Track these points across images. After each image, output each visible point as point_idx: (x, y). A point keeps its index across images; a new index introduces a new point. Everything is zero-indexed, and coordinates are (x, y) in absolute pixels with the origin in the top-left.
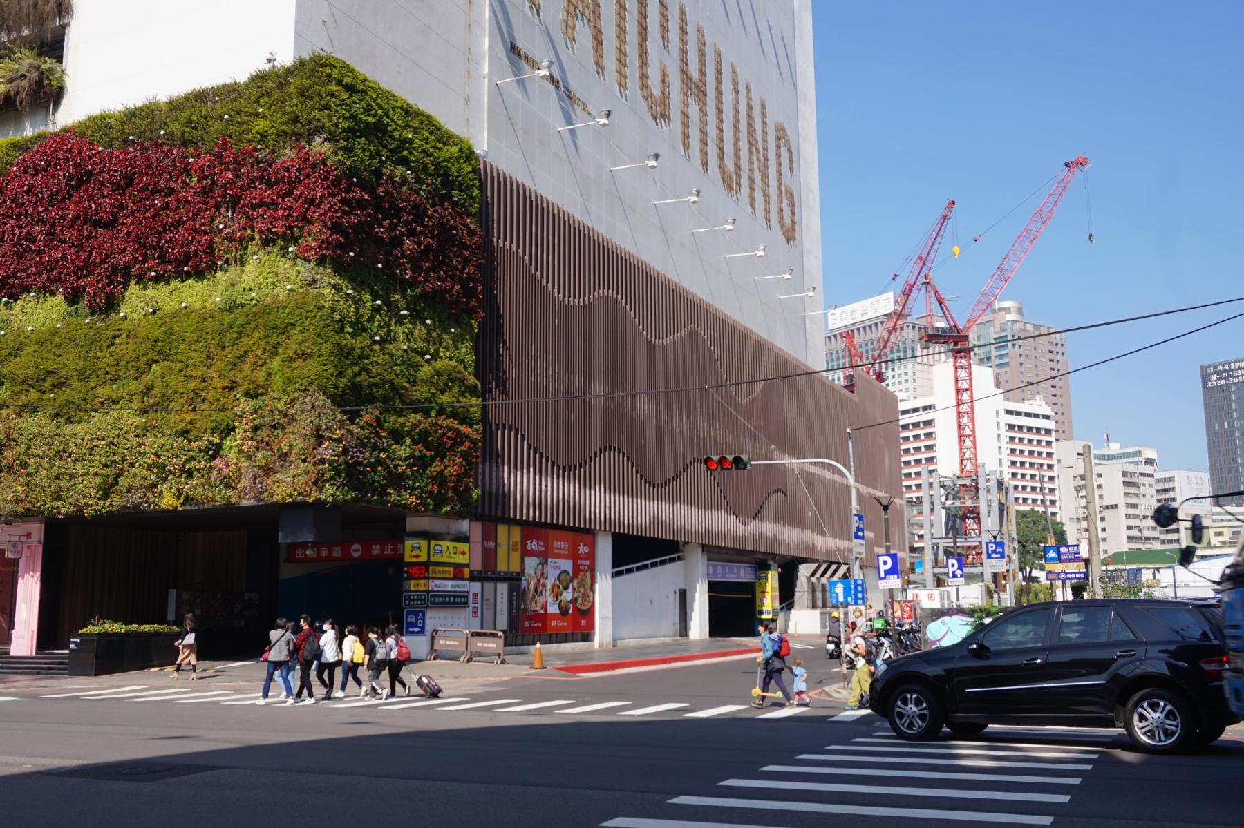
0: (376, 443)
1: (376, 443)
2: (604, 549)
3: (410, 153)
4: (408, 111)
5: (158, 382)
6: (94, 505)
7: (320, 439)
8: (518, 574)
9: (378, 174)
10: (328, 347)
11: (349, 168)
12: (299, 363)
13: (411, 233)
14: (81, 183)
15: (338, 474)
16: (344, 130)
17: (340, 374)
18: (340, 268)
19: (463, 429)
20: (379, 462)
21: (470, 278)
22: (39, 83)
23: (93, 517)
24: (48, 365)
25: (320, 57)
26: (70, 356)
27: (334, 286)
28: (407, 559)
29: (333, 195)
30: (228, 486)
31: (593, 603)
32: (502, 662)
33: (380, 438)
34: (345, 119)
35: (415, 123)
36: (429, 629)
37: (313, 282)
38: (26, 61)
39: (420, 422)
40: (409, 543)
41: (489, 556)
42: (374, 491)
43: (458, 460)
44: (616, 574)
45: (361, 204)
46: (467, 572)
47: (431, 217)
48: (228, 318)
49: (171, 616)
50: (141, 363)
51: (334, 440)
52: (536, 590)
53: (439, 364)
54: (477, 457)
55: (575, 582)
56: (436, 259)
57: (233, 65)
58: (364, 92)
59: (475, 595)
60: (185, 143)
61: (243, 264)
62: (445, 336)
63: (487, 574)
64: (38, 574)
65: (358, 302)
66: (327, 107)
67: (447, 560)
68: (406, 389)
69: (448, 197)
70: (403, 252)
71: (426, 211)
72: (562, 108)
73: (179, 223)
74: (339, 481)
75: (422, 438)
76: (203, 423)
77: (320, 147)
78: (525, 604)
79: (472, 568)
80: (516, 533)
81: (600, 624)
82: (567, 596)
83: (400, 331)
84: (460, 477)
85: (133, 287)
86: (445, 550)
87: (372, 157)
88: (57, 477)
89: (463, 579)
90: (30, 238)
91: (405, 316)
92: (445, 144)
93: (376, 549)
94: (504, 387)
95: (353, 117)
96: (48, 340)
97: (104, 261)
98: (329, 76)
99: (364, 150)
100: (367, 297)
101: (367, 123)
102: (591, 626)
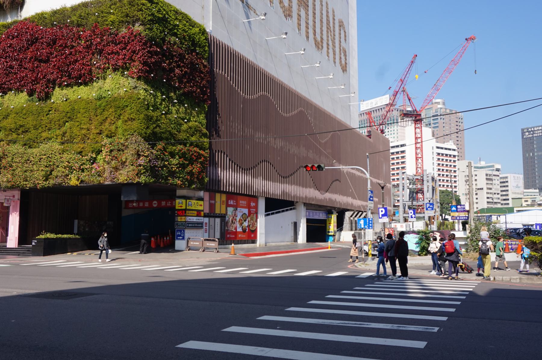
0: (163, 158)
1: (163, 158)
2: (262, 204)
3: (178, 31)
4: (177, 12)
5: (68, 131)
6: (42, 184)
7: (139, 156)
8: (225, 214)
9: (163, 40)
10: (142, 116)
11: (151, 37)
12: (130, 123)
13: (178, 66)
15: (147, 171)
16: (149, 20)
17: (148, 128)
19: (201, 152)
20: (165, 166)
21: (204, 86)
24: (21, 123)
27: (145, 89)
28: (177, 208)
29: (144, 49)
30: (99, 176)
31: (257, 227)
32: (218, 252)
33: (165, 155)
34: (149, 15)
35: (180, 17)
36: (186, 237)
39: (182, 149)
41: (212, 207)
42: (163, 178)
43: (199, 165)
45: (156, 53)
46: (202, 213)
47: (187, 59)
48: (99, 103)
49: (76, 231)
50: (61, 122)
51: (145, 156)
52: (232, 222)
53: (190, 124)
54: (207, 164)
56: (189, 77)
59: (206, 223)
60: (79, 26)
62: (193, 112)
63: (211, 215)
64: (18, 213)
65: (155, 96)
66: (141, 10)
68: (176, 135)
69: (195, 50)
70: (175, 75)
71: (185, 56)
73: (76, 61)
74: (147, 174)
75: (183, 156)
77: (138, 28)
80: (224, 197)
82: (246, 224)
83: (174, 109)
85: (57, 89)
86: (193, 204)
87: (161, 33)
88: (25, 171)
89: (201, 216)
90: (11, 67)
91: (176, 103)
92: (193, 27)
94: (219, 134)
95: (153, 14)
96: (20, 112)
97: (44, 78)
99: (157, 29)
102: (256, 237)
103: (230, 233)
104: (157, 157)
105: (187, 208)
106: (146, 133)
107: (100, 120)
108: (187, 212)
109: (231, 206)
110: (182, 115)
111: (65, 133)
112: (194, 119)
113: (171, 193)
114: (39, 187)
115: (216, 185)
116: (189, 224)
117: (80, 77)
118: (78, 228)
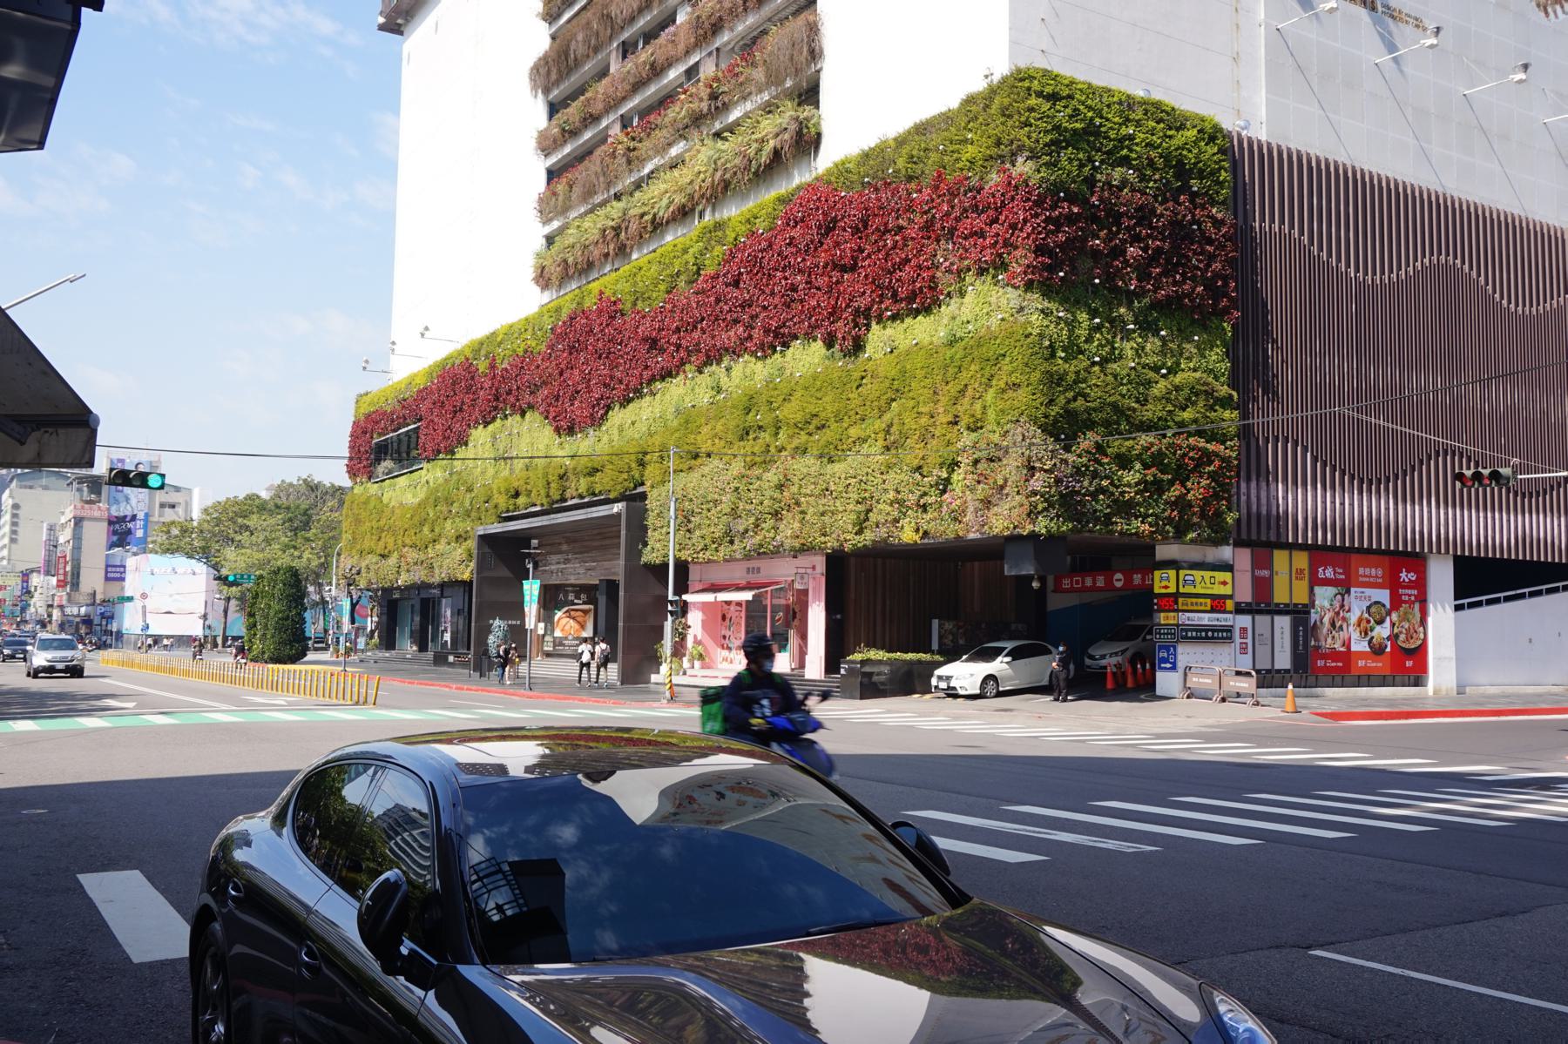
0: (1096, 470)
1: (1096, 470)
2: (1441, 576)
3: (1131, 150)
4: (1129, 103)
5: (896, 421)
6: (853, 541)
7: (1032, 469)
8: (1305, 606)
9: (1090, 182)
10: (1037, 375)
11: (1054, 184)
12: (1010, 394)
13: (1136, 239)
14: (829, 230)
15: (1051, 505)
16: (1046, 145)
17: (1051, 402)
18: (1048, 291)
19: (1211, 447)
20: (1103, 490)
21: (1216, 275)
22: (799, 134)
24: (812, 409)
25: (1019, 71)
26: (827, 399)
27: (1042, 311)
28: (1157, 590)
29: (1036, 216)
30: (955, 519)
31: (1425, 641)
32: (1257, 704)
33: (1102, 465)
34: (1046, 132)
35: (1138, 114)
36: (1181, 665)
37: (1021, 309)
38: (788, 114)
39: (1152, 444)
40: (1157, 574)
41: (1263, 587)
42: (1097, 521)
43: (1204, 482)
44: (1458, 608)
45: (1071, 219)
46: (1230, 604)
47: (1162, 215)
48: (949, 353)
49: (935, 646)
50: (882, 402)
52: (1333, 624)
53: (1178, 379)
54: (1230, 478)
55: (1394, 616)
56: (1168, 261)
57: (944, 97)
58: (1070, 97)
59: (1244, 630)
60: (910, 178)
61: (962, 294)
62: (1187, 346)
63: (1261, 604)
64: (823, 604)
65: (1072, 324)
66: (1027, 124)
68: (1134, 410)
69: (1186, 188)
70: (1126, 262)
71: (1153, 211)
72: (1380, 34)
73: (907, 261)
74: (1053, 512)
75: (1157, 460)
77: (1023, 167)
79: (1238, 599)
80: (1302, 560)
81: (1436, 667)
82: (1383, 632)
83: (1128, 348)
84: (1206, 502)
85: (874, 326)
86: (1199, 579)
87: (1081, 166)
88: (823, 514)
89: (1225, 612)
90: (794, 288)
91: (1134, 331)
92: (1178, 129)
93: (1100, 582)
94: (1275, 393)
95: (1057, 128)
96: (814, 385)
97: (848, 306)
98: (1029, 89)
99: (1070, 160)
100: (1083, 316)
101: (1075, 130)
102: (1422, 667)
103: (1325, 657)
104: (1078, 469)
105: (1182, 590)
106: (1046, 417)
107: (954, 392)
108: (1181, 600)
109: (1327, 582)
110: (1152, 359)
111: (890, 425)
113: (1141, 555)
114: (848, 547)
115: (1269, 528)
117: (911, 298)
118: (941, 637)
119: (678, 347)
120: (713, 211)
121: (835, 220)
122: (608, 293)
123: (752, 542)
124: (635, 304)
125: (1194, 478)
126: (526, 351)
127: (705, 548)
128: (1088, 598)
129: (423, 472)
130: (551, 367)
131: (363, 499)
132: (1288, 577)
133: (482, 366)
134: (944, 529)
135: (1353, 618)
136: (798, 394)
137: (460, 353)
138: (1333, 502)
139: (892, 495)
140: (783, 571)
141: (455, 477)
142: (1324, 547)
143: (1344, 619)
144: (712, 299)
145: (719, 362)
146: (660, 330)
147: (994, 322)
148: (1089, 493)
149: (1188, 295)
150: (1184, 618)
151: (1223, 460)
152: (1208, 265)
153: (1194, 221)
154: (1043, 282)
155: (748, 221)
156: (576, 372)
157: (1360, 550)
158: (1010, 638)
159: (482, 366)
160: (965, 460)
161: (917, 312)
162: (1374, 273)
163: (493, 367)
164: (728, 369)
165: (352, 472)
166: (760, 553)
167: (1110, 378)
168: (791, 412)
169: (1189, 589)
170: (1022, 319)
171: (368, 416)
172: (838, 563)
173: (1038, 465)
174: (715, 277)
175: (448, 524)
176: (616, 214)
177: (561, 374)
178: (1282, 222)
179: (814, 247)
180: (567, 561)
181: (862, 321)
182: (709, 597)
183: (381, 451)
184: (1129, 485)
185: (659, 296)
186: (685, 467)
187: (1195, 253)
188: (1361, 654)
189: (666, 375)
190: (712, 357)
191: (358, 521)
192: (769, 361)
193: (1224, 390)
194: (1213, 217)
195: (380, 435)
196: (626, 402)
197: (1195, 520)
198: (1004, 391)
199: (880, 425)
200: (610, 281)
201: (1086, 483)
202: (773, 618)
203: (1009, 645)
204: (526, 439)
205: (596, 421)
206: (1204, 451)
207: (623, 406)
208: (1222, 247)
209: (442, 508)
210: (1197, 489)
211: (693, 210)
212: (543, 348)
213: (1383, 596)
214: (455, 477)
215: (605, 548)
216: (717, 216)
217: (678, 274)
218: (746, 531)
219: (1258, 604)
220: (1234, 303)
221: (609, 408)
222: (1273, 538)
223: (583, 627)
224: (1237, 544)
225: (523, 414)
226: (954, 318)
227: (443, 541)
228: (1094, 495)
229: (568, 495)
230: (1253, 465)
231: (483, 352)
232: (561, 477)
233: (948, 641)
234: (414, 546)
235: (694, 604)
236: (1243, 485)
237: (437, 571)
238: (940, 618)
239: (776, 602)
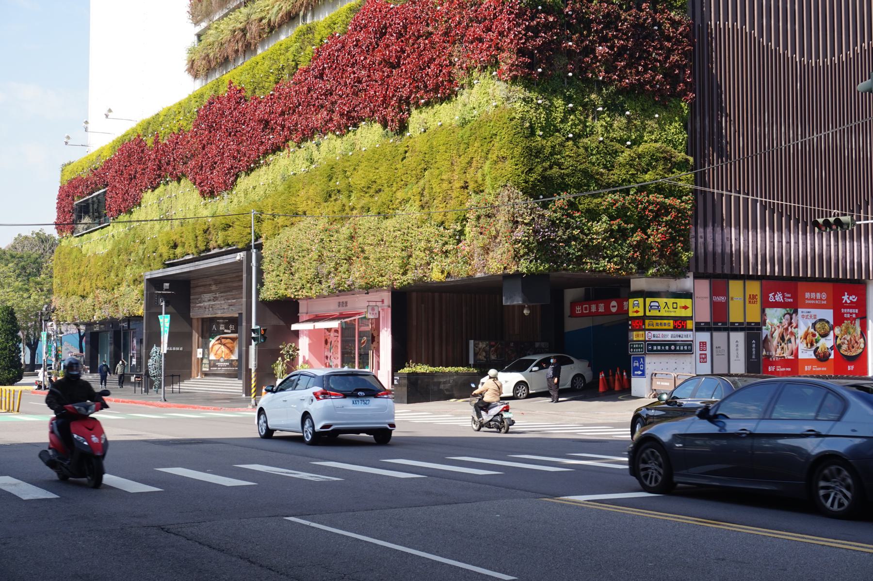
8: (757, 324)
10: (518, 151)
12: (500, 165)
13: (604, 40)
15: (530, 250)
17: (531, 170)
18: (529, 83)
20: (575, 238)
21: (675, 65)
23: (401, 288)
24: (372, 177)
27: (524, 99)
28: (631, 314)
36: (648, 372)
37: (508, 99)
39: (616, 201)
40: (631, 301)
41: (720, 311)
42: (570, 261)
43: (662, 229)
45: (547, 27)
47: (626, 20)
49: (471, 362)
50: (418, 171)
51: (526, 224)
52: (782, 338)
55: (837, 330)
56: (632, 56)
59: (703, 344)
61: (471, 86)
62: (649, 122)
63: (719, 322)
64: (390, 330)
65: (549, 110)
67: (663, 313)
68: (602, 174)
71: (619, 16)
73: (432, 60)
74: (532, 256)
75: (622, 213)
76: (451, 216)
78: (768, 350)
79: (698, 319)
82: (826, 343)
84: (663, 245)
85: (414, 112)
86: (662, 305)
89: (686, 330)
96: (375, 157)
97: (393, 96)
100: (559, 102)
105: (648, 314)
106: (526, 182)
108: (647, 322)
111: (423, 190)
112: (653, 137)
113: (616, 289)
115: (723, 263)
116: (652, 345)
117: (436, 89)
118: (475, 354)
119: (283, 127)
120: (313, 15)
121: (385, 27)
122: (235, 83)
123: (333, 282)
124: (254, 92)
125: (654, 226)
126: (180, 130)
127: (303, 288)
128: (599, 321)
129: (110, 228)
130: (195, 143)
131: (67, 250)
132: (741, 300)
133: (149, 141)
134: (461, 271)
135: (801, 332)
136: (363, 165)
137: (134, 130)
138: (780, 242)
139: (423, 244)
140: (360, 304)
141: (132, 232)
142: (772, 277)
143: (792, 334)
144: (305, 88)
145: (312, 139)
146: (271, 113)
147: (490, 109)
148: (565, 241)
149: (649, 82)
150: (650, 336)
151: (679, 211)
152: (667, 57)
153: (655, 22)
154: (524, 77)
155: (329, 26)
156: (214, 147)
157: (805, 279)
158: (535, 353)
159: (149, 141)
160: (471, 216)
161: (442, 101)
162: (818, 57)
163: (156, 142)
164: (318, 145)
165: (59, 226)
166: (340, 291)
167: (582, 150)
168: (358, 179)
169: (655, 313)
170: (509, 107)
171: (70, 182)
172: (401, 299)
173: (520, 219)
174: (307, 71)
175: (128, 270)
176: (242, 18)
177: (204, 149)
178: (735, 19)
179: (371, 49)
180: (215, 299)
181: (405, 107)
182: (309, 326)
183: (84, 210)
184: (597, 233)
185: (270, 84)
186: (288, 223)
187: (655, 48)
188: (808, 361)
189: (276, 149)
190: (307, 135)
191: (64, 269)
192: (345, 138)
193: (681, 156)
194: (671, 19)
195: (79, 197)
196: (249, 171)
197: (654, 259)
198: (496, 162)
199: (416, 189)
200: (239, 73)
201: (560, 233)
202: (359, 341)
203: (538, 358)
204: (181, 201)
205: (229, 186)
206: (662, 205)
207: (247, 174)
208: (678, 42)
209: (123, 257)
210: (656, 235)
211: (297, 15)
212: (191, 127)
213: (828, 315)
214: (132, 232)
215: (230, 289)
216: (315, 20)
217: (283, 68)
218: (330, 273)
219: (716, 323)
220: (690, 87)
221: (237, 176)
222: (727, 271)
223: (232, 351)
224: (696, 277)
225: (179, 180)
226: (465, 105)
227: (125, 284)
228: (567, 242)
229: (211, 246)
230: (707, 211)
231: (150, 130)
232: (205, 231)
233: (482, 357)
234: (104, 288)
235: (303, 331)
236: (701, 230)
237: (121, 309)
238: (475, 340)
239: (363, 329)
